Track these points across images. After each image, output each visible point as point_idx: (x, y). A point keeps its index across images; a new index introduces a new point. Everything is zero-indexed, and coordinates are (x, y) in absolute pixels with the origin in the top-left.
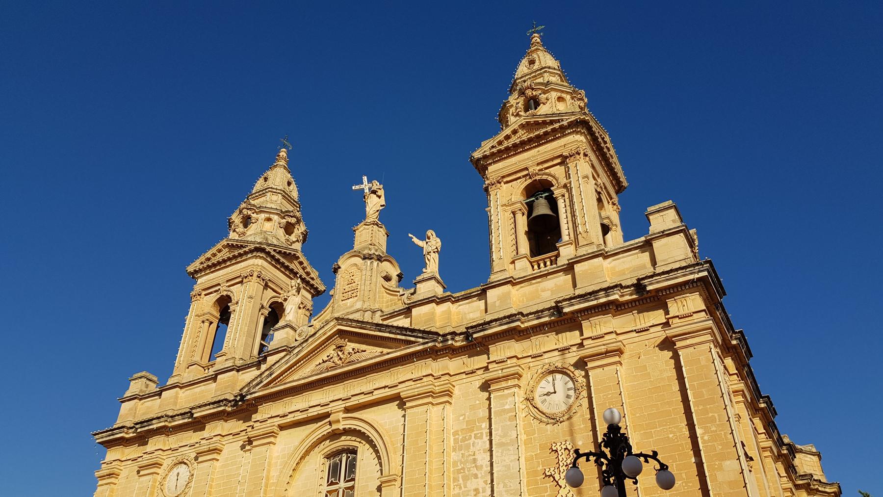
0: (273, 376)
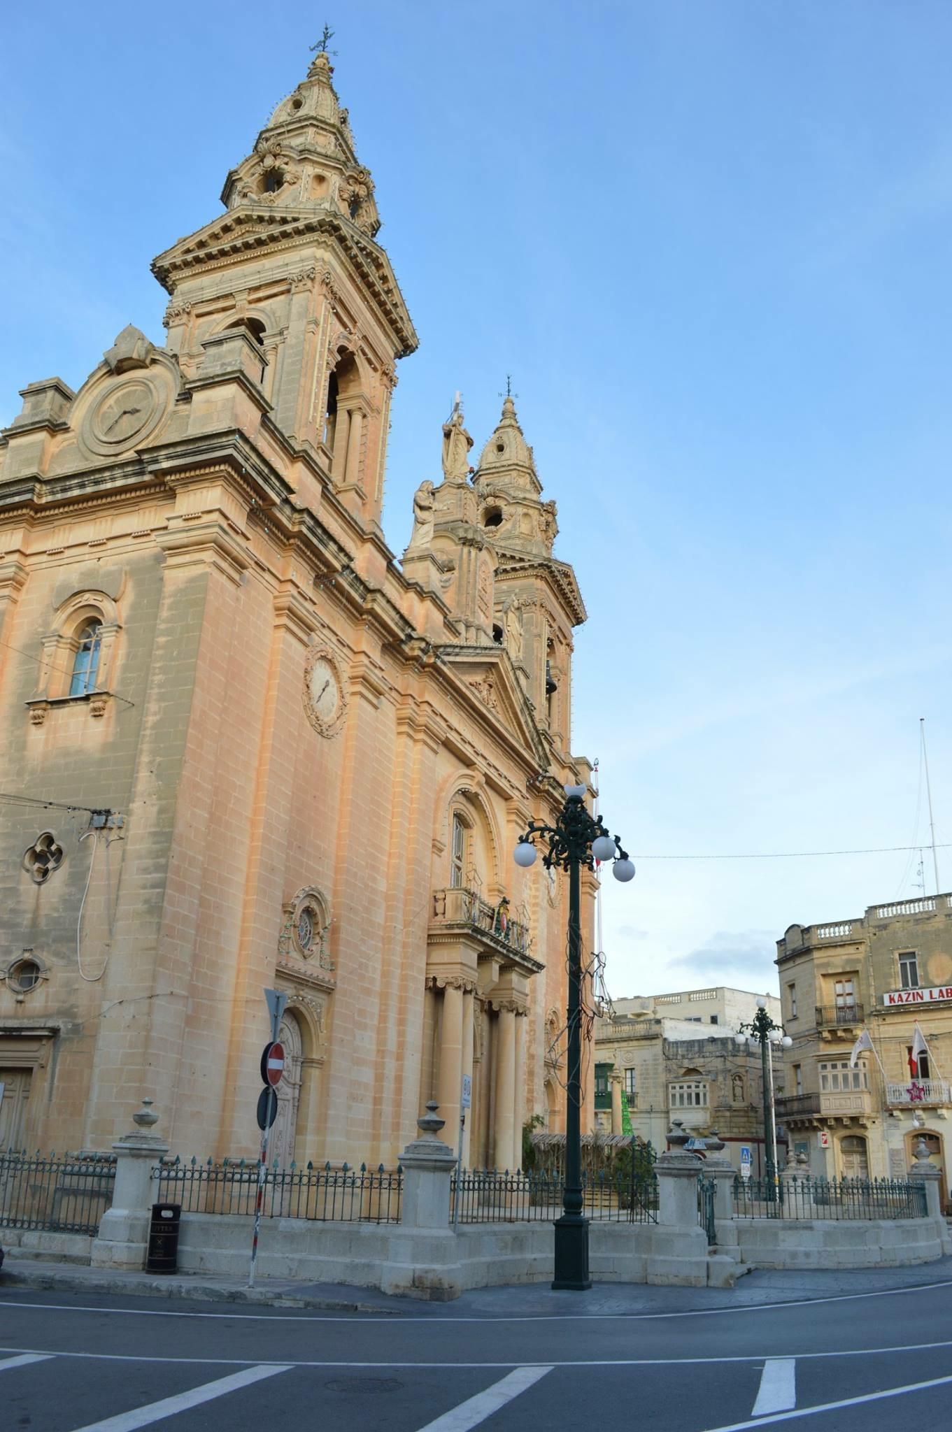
0: (458, 659)
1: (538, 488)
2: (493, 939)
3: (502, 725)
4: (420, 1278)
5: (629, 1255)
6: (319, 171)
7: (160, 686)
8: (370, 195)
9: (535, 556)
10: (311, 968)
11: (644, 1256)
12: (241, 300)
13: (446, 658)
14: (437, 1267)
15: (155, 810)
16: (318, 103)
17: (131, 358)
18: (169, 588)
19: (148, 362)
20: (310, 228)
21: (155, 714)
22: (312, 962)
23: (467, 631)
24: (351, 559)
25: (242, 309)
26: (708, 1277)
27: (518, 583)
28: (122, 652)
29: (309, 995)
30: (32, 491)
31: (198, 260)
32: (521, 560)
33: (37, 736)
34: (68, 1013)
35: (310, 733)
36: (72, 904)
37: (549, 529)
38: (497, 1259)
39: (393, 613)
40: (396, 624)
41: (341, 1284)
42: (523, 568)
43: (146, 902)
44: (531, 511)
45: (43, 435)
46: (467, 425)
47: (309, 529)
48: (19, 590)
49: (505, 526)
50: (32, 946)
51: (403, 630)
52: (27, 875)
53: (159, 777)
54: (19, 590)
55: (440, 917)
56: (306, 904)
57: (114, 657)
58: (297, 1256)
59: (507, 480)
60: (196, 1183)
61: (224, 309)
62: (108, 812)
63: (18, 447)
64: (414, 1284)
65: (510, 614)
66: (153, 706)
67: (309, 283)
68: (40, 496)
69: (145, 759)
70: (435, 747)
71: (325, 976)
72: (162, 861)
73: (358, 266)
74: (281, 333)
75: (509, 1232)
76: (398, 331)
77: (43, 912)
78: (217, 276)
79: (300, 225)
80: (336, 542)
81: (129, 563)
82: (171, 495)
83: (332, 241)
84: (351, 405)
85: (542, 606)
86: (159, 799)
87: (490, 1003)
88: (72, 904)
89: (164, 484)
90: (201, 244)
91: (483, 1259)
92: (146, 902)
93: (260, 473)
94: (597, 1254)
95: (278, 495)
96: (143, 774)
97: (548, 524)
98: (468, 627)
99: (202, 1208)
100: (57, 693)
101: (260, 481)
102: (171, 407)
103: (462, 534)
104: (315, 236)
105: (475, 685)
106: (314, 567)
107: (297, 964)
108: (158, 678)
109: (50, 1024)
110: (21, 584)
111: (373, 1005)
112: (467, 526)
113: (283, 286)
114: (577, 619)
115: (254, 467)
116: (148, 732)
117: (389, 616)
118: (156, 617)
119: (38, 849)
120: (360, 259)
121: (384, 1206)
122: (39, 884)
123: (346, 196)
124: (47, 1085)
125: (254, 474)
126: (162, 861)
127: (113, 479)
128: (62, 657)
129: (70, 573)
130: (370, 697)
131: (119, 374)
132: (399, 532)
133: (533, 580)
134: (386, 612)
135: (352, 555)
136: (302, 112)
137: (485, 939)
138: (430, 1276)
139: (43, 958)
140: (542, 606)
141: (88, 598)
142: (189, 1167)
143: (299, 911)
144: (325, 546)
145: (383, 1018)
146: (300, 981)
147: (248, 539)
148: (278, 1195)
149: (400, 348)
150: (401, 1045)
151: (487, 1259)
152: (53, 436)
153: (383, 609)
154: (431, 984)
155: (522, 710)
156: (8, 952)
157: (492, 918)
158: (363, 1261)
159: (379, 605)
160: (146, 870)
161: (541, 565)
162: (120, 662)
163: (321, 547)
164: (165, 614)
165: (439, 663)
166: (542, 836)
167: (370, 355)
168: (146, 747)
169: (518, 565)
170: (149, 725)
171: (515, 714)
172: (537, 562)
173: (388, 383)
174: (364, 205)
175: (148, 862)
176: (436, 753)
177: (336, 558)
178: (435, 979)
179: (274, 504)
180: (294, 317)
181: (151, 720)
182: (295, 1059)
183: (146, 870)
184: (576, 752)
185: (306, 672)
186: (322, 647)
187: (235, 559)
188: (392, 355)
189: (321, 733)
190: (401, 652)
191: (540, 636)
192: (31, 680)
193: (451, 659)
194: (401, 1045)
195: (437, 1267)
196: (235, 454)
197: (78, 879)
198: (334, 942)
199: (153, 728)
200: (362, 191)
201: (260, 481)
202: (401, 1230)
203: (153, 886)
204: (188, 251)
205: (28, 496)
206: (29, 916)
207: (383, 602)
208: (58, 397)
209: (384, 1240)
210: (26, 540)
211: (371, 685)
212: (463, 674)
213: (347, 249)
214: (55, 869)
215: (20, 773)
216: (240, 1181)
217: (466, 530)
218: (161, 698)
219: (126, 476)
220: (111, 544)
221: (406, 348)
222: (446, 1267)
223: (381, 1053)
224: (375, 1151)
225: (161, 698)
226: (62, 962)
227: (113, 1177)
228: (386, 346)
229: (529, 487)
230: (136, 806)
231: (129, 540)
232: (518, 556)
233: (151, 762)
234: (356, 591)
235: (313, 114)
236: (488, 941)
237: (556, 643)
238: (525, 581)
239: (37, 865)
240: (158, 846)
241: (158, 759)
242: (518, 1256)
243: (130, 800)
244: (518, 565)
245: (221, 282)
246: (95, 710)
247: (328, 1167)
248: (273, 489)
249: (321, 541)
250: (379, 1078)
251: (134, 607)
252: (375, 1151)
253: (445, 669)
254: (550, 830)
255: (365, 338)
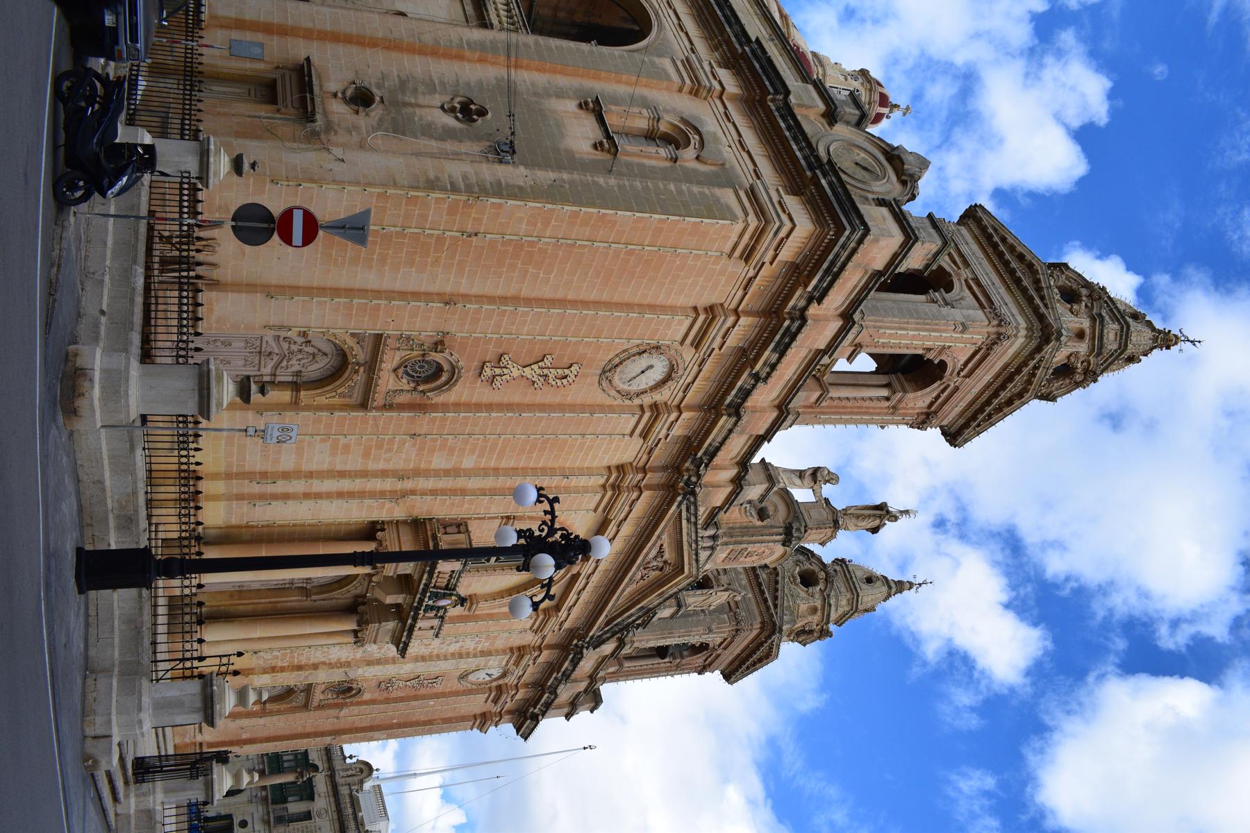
0: (684, 522)
1: (839, 622)
2: (427, 586)
3: (624, 590)
4: (85, 375)
5: (117, 654)
6: (1088, 331)
7: (632, 186)
8: (1078, 385)
9: (782, 618)
10: (387, 381)
11: (116, 670)
12: (965, 273)
13: (684, 507)
14: (97, 392)
15: (521, 184)
16: (1140, 336)
17: (903, 164)
18: (718, 192)
19: (904, 178)
20: (1041, 318)
21: (607, 183)
22: (391, 381)
23: (709, 537)
24: (765, 380)
25: (958, 275)
26: (95, 737)
27: (754, 607)
28: (654, 163)
29: (360, 378)
30: (777, 92)
31: (989, 237)
32: (776, 606)
33: (571, 105)
34: (329, 127)
35: (604, 357)
36: (428, 131)
37: (803, 635)
38: (109, 494)
39: (719, 439)
40: (710, 445)
41: (79, 315)
42: (768, 608)
43: (437, 178)
44: (819, 613)
45: (822, 107)
46: (889, 525)
47: (788, 328)
48: (690, 93)
49: (801, 591)
50: (386, 103)
51: (705, 453)
52: (448, 98)
53: (550, 186)
54: (690, 93)
55: (442, 530)
56: (446, 367)
57: (649, 158)
58: (107, 278)
59: (843, 589)
60: (176, 460)
61: (954, 262)
62: (514, 152)
63: (807, 90)
64: (78, 369)
65: (727, 594)
66: (612, 181)
67: (995, 322)
68: (773, 100)
69: (565, 176)
70: (600, 509)
71: (379, 399)
72: (476, 189)
73: (1018, 371)
74: (947, 304)
75: (136, 511)
76: (966, 425)
77: (418, 111)
78: (980, 254)
79: (1043, 309)
80: (779, 360)
81: (732, 167)
82: (795, 190)
83: (1034, 344)
84: (896, 384)
85: (737, 630)
86: (531, 187)
87: (364, 604)
88: (428, 131)
89: (805, 186)
90: (1004, 240)
91: (107, 475)
92: (437, 178)
93: (833, 263)
94: (119, 600)
95: (815, 288)
96: (552, 175)
97: (811, 632)
98: (714, 538)
99: (153, 208)
100: (611, 120)
101: (825, 266)
102: (870, 196)
103: (795, 526)
104: (1037, 325)
105: (661, 552)
106: (753, 344)
107: (390, 359)
108: (638, 184)
109: (318, 117)
110: (696, 95)
111: (353, 462)
112: (803, 529)
113: (985, 301)
114: (730, 675)
115: (837, 256)
116: (589, 178)
117: (717, 435)
118: (691, 182)
119: (473, 107)
120: (1025, 370)
121: (162, 489)
122: (442, 107)
123: (1072, 359)
124: (263, 114)
125: (831, 257)
126: (476, 189)
127: (801, 149)
128: (642, 124)
129: (710, 124)
130: (641, 426)
131: (887, 159)
132: (789, 450)
133: (759, 620)
134: (720, 431)
135: (769, 380)
136: (1130, 320)
137: (425, 576)
138: (86, 384)
139: (376, 111)
140: (737, 630)
141: (694, 139)
142: (191, 345)
143: (437, 357)
144: (774, 350)
145: (342, 474)
146: (372, 366)
147: (771, 263)
148: (169, 344)
149: (953, 430)
150: (318, 496)
151: (108, 483)
152: (823, 115)
153: (722, 427)
154: (379, 527)
155: (642, 608)
156: (379, 87)
157: (446, 588)
158: (103, 333)
159: (726, 421)
160: (465, 177)
161: (774, 624)
162: (646, 162)
163: (772, 345)
164: (695, 189)
165: (679, 498)
166: (546, 512)
167: (943, 396)
168: (576, 176)
169: (770, 603)
170: (596, 179)
171: (638, 602)
172: (777, 620)
173: (920, 419)
174: (1068, 381)
175: (473, 179)
176: (595, 510)
177: (764, 364)
178: (383, 530)
179: (806, 286)
180: (964, 312)
181: (601, 180)
182: (298, 374)
183: (465, 177)
184: (606, 689)
185: (658, 348)
186: (681, 366)
187: (753, 249)
188: (945, 423)
189: (604, 372)
190: (684, 460)
191: (710, 631)
192: (616, 101)
193: (684, 514)
194: (318, 496)
195: (97, 392)
196: (847, 233)
197: (448, 134)
198: (411, 407)
199: (594, 182)
200: (1079, 378)
201: (825, 266)
202: (135, 363)
203: (452, 184)
204: (995, 230)
205: (771, 90)
206: (413, 101)
207: (729, 426)
208: (857, 118)
209: (126, 350)
210: (733, 98)
211: (652, 425)
212: (670, 535)
213: (1031, 356)
214: (457, 118)
215: (535, 94)
216: (181, 297)
217: (798, 530)
218: (620, 187)
219: (805, 158)
220: (745, 155)
221: (954, 436)
222: (96, 403)
223: (310, 475)
224: (215, 476)
225: (620, 187)
226: (375, 123)
227: (182, 138)
228: (953, 412)
229: (841, 611)
230: (522, 170)
231: (751, 167)
232: (779, 602)
233: (563, 180)
234: (736, 396)
235: (1132, 329)
236: (424, 581)
237: (704, 654)
238: (757, 612)
239: (458, 106)
240: (489, 186)
241: (567, 186)
242: (112, 523)
243: (526, 166)
244: (770, 603)
245: (977, 258)
246: (601, 143)
247: (197, 436)
248: (820, 281)
249: (778, 343)
250: (286, 476)
251: (695, 171)
252: (215, 476)
253: (674, 507)
254: (553, 521)
255: (956, 389)
